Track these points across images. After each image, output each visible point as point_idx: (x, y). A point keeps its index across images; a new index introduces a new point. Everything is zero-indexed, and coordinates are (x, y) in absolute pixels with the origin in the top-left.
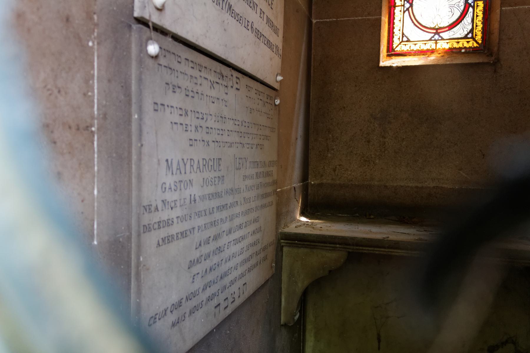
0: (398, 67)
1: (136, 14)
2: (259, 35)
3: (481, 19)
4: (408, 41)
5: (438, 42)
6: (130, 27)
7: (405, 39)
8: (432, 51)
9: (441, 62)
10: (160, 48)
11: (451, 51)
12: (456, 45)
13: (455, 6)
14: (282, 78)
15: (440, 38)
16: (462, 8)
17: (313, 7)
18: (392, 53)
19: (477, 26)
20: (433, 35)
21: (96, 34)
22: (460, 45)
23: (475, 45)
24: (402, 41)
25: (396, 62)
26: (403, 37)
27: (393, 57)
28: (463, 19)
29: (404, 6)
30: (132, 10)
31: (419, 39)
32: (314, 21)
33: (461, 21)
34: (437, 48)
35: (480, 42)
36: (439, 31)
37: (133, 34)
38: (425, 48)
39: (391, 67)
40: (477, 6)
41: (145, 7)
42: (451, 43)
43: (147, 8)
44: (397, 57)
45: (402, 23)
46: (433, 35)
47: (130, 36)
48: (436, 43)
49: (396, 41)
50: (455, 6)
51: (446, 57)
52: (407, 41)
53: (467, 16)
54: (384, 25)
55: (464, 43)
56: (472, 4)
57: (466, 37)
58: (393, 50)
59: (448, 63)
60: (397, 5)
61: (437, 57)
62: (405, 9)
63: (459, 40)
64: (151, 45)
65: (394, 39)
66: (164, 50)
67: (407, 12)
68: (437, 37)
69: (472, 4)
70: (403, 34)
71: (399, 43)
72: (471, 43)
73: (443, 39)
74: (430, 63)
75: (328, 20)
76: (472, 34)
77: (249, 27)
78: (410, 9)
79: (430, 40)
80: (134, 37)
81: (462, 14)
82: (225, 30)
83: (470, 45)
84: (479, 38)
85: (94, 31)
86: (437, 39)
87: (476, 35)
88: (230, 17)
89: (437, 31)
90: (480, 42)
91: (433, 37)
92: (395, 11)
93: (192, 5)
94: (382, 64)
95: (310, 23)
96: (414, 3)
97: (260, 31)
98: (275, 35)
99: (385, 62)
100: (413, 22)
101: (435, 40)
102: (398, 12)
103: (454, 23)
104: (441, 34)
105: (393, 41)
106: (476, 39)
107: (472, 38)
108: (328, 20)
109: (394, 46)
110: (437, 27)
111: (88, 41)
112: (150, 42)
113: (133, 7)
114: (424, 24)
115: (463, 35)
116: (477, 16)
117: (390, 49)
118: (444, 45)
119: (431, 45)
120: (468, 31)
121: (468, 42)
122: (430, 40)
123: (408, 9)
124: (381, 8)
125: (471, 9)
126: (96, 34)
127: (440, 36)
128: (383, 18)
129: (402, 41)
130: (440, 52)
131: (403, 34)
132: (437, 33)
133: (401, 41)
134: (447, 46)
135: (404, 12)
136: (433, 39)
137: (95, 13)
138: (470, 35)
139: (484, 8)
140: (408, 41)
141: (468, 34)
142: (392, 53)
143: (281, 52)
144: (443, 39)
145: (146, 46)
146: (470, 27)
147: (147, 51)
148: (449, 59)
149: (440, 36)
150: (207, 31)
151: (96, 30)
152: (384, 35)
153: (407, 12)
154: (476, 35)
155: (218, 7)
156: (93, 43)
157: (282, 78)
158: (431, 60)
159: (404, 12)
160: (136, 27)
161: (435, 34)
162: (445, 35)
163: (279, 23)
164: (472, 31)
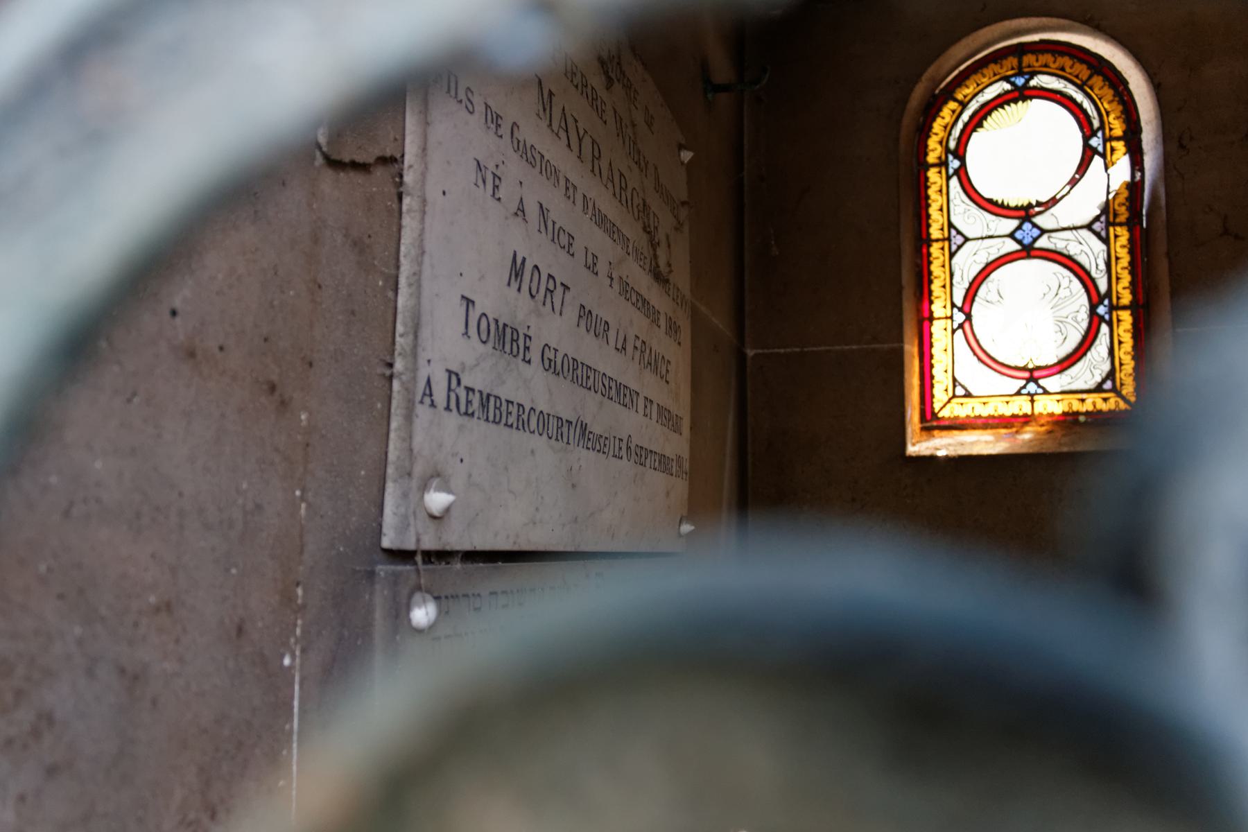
0: (948, 460)
1: (386, 543)
2: (641, 455)
3: (1130, 371)
4: (968, 395)
5: (1036, 398)
6: (371, 575)
7: (960, 391)
8: (1026, 419)
9: (1050, 447)
10: (437, 598)
11: (1068, 421)
12: (1077, 406)
13: (1069, 320)
14: (693, 528)
15: (1040, 391)
16: (1085, 325)
17: (747, 323)
18: (932, 423)
19: (1121, 365)
20: (1024, 382)
21: (298, 631)
22: (1088, 406)
23: (1122, 405)
24: (954, 396)
25: (943, 445)
26: (954, 386)
27: (936, 432)
28: (1089, 349)
29: (951, 318)
30: (379, 532)
31: (994, 394)
32: (750, 353)
33: (1085, 354)
34: (1036, 412)
35: (1133, 399)
36: (1036, 374)
37: (378, 587)
38: (1008, 411)
39: (932, 458)
40: (1119, 321)
41: (409, 525)
42: (1066, 403)
43: (412, 529)
44: (944, 433)
45: (949, 353)
46: (1024, 382)
47: (372, 594)
48: (1032, 401)
49: (940, 396)
50: (1069, 320)
51: (1059, 434)
52: (965, 396)
53: (1097, 342)
54: (912, 363)
55: (1093, 403)
56: (1107, 317)
57: (1098, 389)
58: (934, 415)
59: (1065, 449)
60: (935, 315)
61: (1038, 433)
62: (955, 326)
63: (1084, 396)
64: (420, 607)
65: (935, 391)
66: (446, 597)
67: (960, 332)
68: (1032, 387)
69: (1107, 317)
70: (954, 380)
71: (946, 399)
72: (1112, 401)
73: (1046, 392)
74: (1024, 450)
75: (782, 351)
76: (1114, 381)
77: (623, 453)
78: (967, 326)
79: (1018, 393)
80: (380, 598)
81: (1085, 338)
82: (573, 486)
83: (1111, 405)
84: (1128, 390)
85: (295, 625)
86: (1033, 392)
87: (1122, 385)
88: (585, 452)
89: (1033, 374)
90: (1133, 399)
91: (1024, 387)
92: (933, 329)
93: (506, 469)
94: (913, 449)
95: (742, 357)
96: (973, 313)
97: (645, 446)
98: (676, 436)
99: (918, 446)
100: (975, 354)
101: (1029, 394)
102: (939, 331)
103: (1068, 357)
104: (1041, 382)
105: (932, 396)
106: (1124, 392)
107: (1114, 390)
108: (782, 351)
109: (937, 406)
110: (1030, 366)
111: (282, 657)
112: (418, 597)
113: (380, 526)
114: (1001, 360)
115: (1091, 384)
116: (1120, 343)
117: (929, 417)
118: (1050, 406)
119: (1020, 406)
120: (1104, 375)
121: (1105, 400)
122: (1018, 393)
123: (961, 326)
124: (901, 314)
125: (1104, 328)
126: (298, 631)
127: (1039, 386)
128: (907, 347)
129: (954, 396)
130: (1042, 421)
131: (954, 380)
132: (1032, 379)
133: (951, 394)
134: (1058, 409)
135: (954, 331)
136: (1024, 391)
137: (298, 584)
138: (1108, 385)
139: (1135, 325)
140: (968, 395)
141: (1104, 381)
142: (932, 423)
143: (686, 466)
144: (1046, 392)
145: (408, 609)
146: (1106, 367)
147: (409, 620)
148: (1064, 440)
149: (1039, 386)
150: (537, 509)
151: (299, 622)
152: (911, 385)
153: (960, 332)
154: (1122, 385)
155: (560, 444)
156: (293, 657)
157: (693, 528)
158: (1025, 443)
159: (954, 331)
160: (383, 569)
161: (1028, 380)
162: (1048, 383)
163: (682, 409)
164: (1111, 375)
